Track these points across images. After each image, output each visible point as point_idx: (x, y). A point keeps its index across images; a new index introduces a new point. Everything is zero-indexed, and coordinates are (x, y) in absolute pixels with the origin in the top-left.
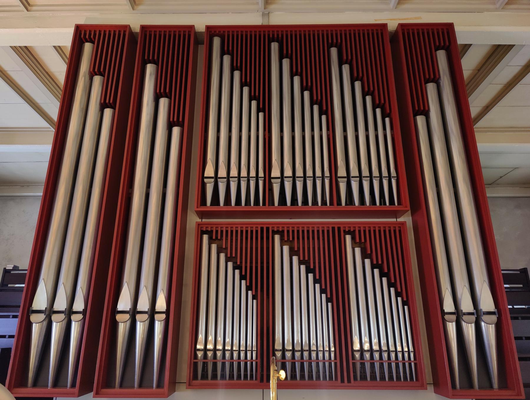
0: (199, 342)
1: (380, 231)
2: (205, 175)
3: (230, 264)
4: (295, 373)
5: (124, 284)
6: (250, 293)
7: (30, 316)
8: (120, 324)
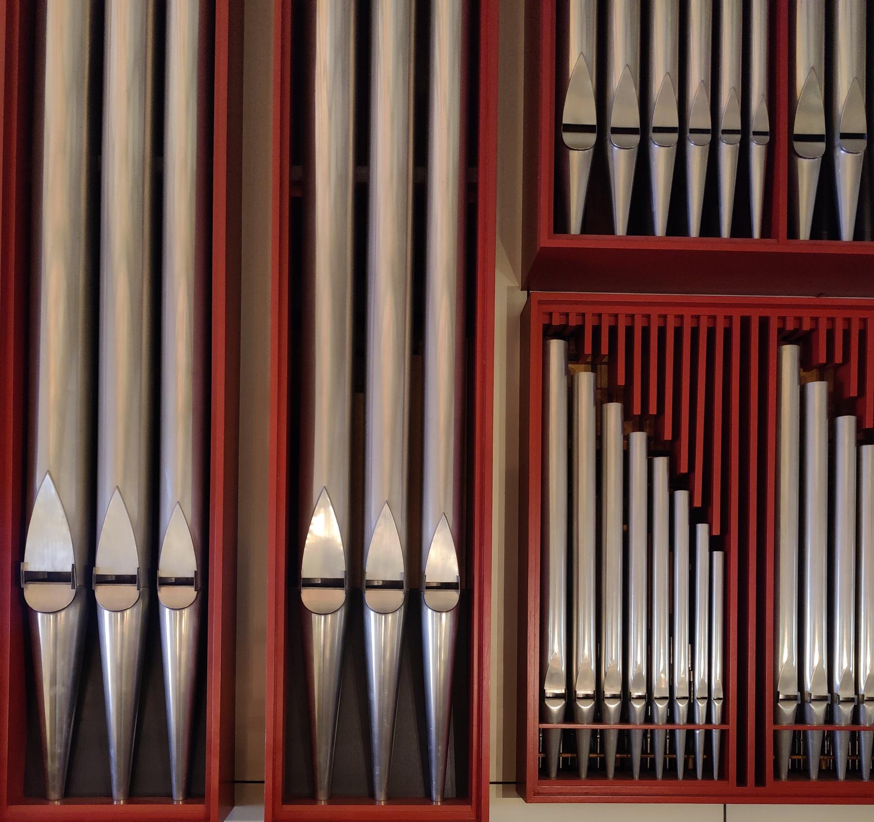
0: (552, 675)
1: (678, 332)
2: (566, 120)
3: (639, 440)
4: (671, 756)
5: (108, 497)
6: (702, 530)
7: (93, 592)
8: (315, 617)
